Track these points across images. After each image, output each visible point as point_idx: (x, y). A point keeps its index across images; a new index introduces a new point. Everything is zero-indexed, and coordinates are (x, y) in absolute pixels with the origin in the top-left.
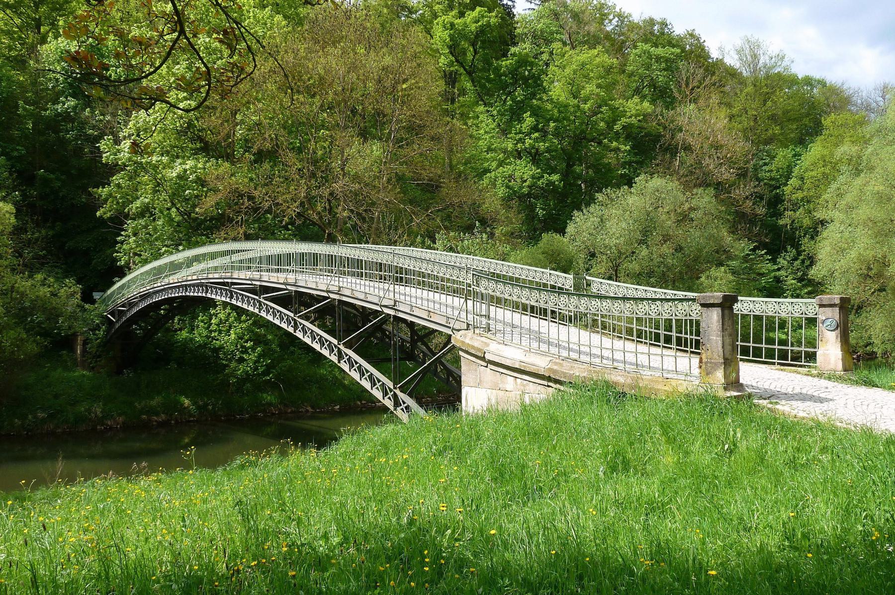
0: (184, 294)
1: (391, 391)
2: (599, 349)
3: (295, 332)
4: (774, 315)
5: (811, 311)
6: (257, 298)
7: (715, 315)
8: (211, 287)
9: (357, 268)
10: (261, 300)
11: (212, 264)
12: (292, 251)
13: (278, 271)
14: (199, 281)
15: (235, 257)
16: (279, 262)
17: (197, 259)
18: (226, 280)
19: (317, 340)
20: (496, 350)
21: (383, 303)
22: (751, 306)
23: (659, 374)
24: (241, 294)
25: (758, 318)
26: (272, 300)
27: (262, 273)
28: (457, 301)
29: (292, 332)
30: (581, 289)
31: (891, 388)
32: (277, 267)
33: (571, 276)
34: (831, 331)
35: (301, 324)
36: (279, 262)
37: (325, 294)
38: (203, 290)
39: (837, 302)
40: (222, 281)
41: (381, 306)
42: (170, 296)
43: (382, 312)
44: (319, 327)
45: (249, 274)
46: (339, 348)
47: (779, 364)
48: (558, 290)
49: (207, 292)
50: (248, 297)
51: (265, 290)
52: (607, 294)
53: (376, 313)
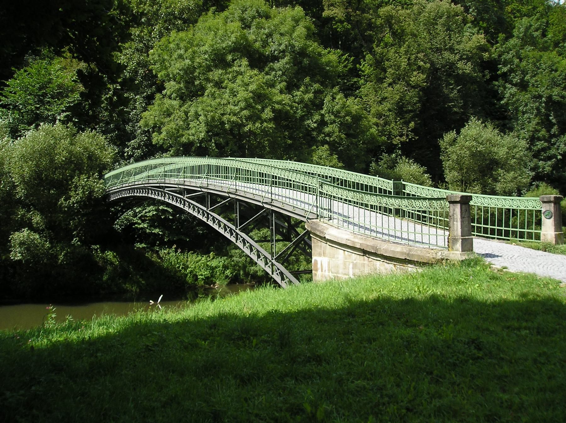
0: (133, 195)
1: (270, 261)
2: (394, 231)
3: (184, 207)
4: (502, 207)
5: (538, 206)
6: (182, 197)
7: (458, 208)
8: (151, 189)
9: (238, 174)
10: (185, 198)
11: (152, 173)
12: (192, 164)
13: (192, 177)
14: (143, 185)
15: (161, 170)
16: (197, 170)
17: (146, 168)
18: (161, 185)
19: (216, 222)
20: (331, 233)
21: (264, 201)
22: (504, 202)
23: (428, 247)
24: (171, 195)
25: (500, 210)
26: (191, 198)
27: (185, 179)
28: (310, 198)
29: (183, 208)
30: (399, 192)
31: (563, 252)
32: (191, 175)
33: (392, 182)
34: (549, 219)
35: (211, 216)
36: (197, 170)
37: (227, 195)
38: (146, 191)
39: (552, 199)
40: (158, 185)
41: (263, 203)
42: (123, 196)
43: (263, 207)
44: (224, 218)
45: (176, 180)
46: (236, 232)
47: (498, 239)
48: (383, 192)
49: (148, 193)
50: (198, 208)
51: (189, 191)
52: (427, 197)
53: (224, 198)
